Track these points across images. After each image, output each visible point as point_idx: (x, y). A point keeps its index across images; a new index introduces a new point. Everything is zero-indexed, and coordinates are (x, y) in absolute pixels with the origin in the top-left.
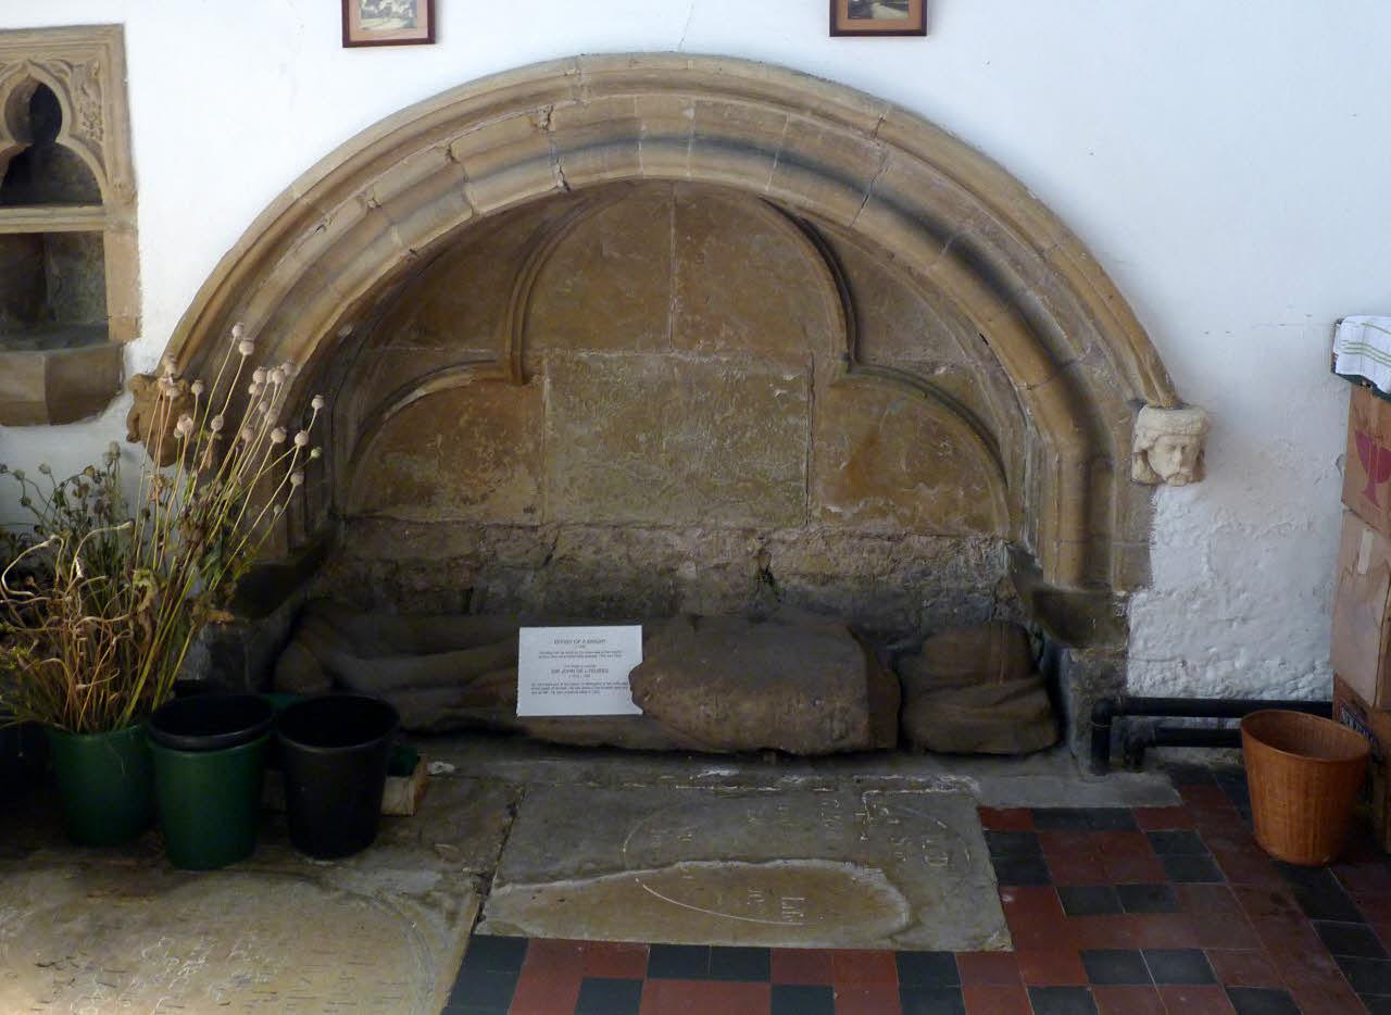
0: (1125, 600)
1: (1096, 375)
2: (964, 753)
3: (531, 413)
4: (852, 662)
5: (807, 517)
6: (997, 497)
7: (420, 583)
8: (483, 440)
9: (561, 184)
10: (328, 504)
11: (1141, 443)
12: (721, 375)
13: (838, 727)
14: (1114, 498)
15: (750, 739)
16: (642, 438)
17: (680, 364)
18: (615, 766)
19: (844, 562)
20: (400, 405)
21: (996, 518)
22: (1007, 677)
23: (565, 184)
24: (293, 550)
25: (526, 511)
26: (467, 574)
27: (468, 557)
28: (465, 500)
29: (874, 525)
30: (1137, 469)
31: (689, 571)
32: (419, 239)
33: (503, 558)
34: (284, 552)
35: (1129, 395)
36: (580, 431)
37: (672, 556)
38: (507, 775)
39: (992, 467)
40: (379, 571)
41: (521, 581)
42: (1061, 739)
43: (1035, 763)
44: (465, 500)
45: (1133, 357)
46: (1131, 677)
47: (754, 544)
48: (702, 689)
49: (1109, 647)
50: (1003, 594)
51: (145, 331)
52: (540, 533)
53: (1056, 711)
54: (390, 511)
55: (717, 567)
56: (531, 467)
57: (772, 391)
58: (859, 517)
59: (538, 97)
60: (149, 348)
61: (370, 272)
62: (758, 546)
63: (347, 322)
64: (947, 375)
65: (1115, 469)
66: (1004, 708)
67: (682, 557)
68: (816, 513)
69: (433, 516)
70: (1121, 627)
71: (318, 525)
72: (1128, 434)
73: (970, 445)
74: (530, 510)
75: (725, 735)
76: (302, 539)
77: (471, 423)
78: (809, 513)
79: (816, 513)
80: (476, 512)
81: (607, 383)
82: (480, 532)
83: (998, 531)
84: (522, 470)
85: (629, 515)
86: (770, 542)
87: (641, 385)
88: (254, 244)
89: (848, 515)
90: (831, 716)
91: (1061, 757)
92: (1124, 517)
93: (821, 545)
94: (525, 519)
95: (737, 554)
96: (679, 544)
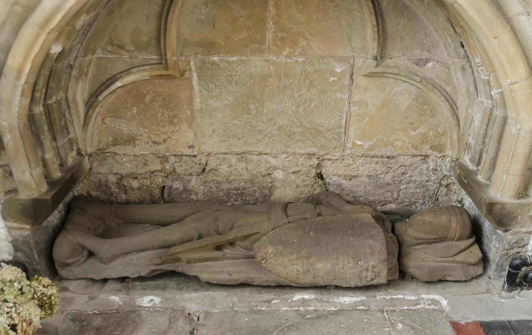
10: (75, 148)
12: (298, 69)
13: (370, 275)
16: (252, 107)
21: (448, 146)
22: (459, 239)
24: (52, 184)
25: (190, 147)
31: (279, 175)
34: (45, 188)
39: (454, 122)
40: (113, 179)
41: (190, 181)
44: (155, 143)
45: (507, 37)
48: (294, 256)
50: (444, 182)
52: (198, 158)
53: (485, 260)
54: (112, 149)
55: (294, 173)
61: (57, 9)
62: (316, 162)
64: (434, 67)
66: (459, 258)
67: (275, 168)
68: (349, 145)
75: (308, 279)
76: (57, 174)
77: (152, 101)
81: (231, 75)
82: (164, 159)
85: (246, 148)
86: (323, 160)
89: (366, 146)
90: (367, 270)
94: (189, 152)
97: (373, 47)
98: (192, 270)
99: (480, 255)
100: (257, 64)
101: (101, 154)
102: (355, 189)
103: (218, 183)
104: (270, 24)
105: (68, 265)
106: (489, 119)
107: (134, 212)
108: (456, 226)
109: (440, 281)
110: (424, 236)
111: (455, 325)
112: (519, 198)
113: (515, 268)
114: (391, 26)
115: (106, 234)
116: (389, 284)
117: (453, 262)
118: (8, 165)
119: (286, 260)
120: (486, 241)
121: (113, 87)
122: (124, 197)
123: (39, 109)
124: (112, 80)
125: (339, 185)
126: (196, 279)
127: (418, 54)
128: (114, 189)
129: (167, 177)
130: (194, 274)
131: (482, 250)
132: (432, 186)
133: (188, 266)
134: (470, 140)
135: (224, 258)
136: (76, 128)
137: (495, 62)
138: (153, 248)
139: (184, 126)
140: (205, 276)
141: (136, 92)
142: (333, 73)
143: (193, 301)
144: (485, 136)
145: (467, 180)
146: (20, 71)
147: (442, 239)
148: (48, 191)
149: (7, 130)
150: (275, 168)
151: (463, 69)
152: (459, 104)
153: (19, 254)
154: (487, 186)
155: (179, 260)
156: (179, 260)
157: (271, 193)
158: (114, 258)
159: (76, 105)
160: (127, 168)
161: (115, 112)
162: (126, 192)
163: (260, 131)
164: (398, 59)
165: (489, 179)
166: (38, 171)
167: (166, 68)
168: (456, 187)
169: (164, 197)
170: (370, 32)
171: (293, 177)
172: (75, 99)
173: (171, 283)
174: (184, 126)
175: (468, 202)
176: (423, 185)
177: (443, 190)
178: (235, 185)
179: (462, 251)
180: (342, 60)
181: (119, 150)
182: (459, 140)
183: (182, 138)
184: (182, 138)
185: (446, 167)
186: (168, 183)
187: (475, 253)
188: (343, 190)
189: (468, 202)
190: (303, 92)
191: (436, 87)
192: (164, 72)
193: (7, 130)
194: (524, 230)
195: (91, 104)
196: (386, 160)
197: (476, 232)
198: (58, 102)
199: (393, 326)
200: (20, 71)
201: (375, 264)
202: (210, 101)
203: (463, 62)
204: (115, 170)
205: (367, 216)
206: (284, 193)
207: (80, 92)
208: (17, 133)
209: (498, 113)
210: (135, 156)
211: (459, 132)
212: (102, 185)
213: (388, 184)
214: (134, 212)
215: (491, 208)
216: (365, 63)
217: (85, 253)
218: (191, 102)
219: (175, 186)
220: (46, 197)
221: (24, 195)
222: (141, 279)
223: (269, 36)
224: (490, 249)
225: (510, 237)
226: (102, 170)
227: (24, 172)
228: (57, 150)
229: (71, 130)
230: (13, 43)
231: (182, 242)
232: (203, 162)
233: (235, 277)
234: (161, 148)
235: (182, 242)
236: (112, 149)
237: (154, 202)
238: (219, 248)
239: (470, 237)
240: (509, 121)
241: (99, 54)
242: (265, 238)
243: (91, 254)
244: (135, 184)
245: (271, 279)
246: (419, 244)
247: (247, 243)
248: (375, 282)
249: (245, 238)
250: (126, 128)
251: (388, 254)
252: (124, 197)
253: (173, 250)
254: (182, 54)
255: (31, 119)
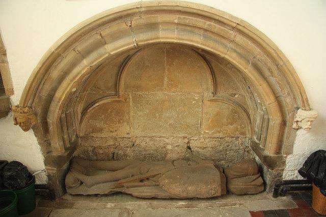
0: (286, 157)
1: (287, 100)
2: (244, 194)
3: (127, 109)
4: (216, 175)
5: (200, 133)
6: (248, 128)
7: (101, 152)
8: (115, 116)
9: (135, 45)
10: (75, 134)
11: (298, 119)
12: (178, 98)
13: (213, 192)
14: (286, 132)
15: (190, 196)
16: (157, 115)
17: (167, 95)
18: (155, 203)
19: (208, 144)
20: (91, 108)
21: (247, 133)
22: (253, 175)
23: (137, 44)
24: (66, 149)
25: (127, 134)
26: (113, 149)
27: (113, 145)
28: (111, 132)
29: (217, 135)
30: (295, 126)
31: (169, 147)
32: (93, 63)
33: (122, 145)
34: (64, 151)
35: (295, 106)
36: (140, 113)
37: (165, 144)
38: (128, 207)
39: (248, 121)
40: (90, 149)
41: (127, 150)
42: (265, 190)
43: (258, 196)
44: (111, 132)
45: (265, 85)
46: (284, 174)
47: (187, 140)
48: (178, 184)
49: (280, 168)
50: (247, 150)
51: (15, 92)
52: (131, 139)
53: (265, 184)
54: (92, 135)
55: (177, 146)
56: (128, 123)
57: (191, 102)
58: (214, 133)
59: (128, 15)
60: (16, 99)
61: (79, 73)
62: (187, 141)
63: (74, 87)
64: (238, 97)
65: (287, 125)
66: (253, 183)
67: (168, 144)
68: (202, 133)
69: (103, 135)
70: (284, 163)
71: (73, 139)
72: (293, 117)
73: (244, 115)
74: (128, 134)
75: (184, 195)
76: (68, 145)
77: (111, 112)
78: (200, 133)
79: (202, 133)
80: (114, 134)
81: (148, 101)
82: (115, 139)
83: (248, 136)
84: (125, 124)
85: (154, 135)
86: (190, 140)
87: (157, 101)
88: (42, 66)
89: (210, 133)
90: (212, 189)
91: (265, 194)
92: (288, 138)
93: (203, 140)
94: (127, 136)
95: (182, 143)
96: (167, 141)
97: (211, 87)
98: (129, 191)
99: (263, 181)
100: (160, 95)
101: (86, 137)
102: (206, 154)
103: (140, 151)
104: (166, 79)
105: (72, 187)
106: (263, 120)
107: (101, 164)
108: (251, 168)
109: (245, 194)
110: (237, 174)
111: (252, 213)
112: (277, 154)
113: (277, 186)
114: (218, 79)
115: (88, 174)
116: (222, 196)
117: (250, 185)
118: (49, 140)
119: (174, 185)
120: (265, 175)
121: (94, 106)
122: (95, 158)
123: (64, 115)
124: (94, 103)
125: (198, 152)
126: (131, 195)
127: (231, 91)
128: (91, 154)
129: (116, 148)
130: (130, 193)
131: (263, 180)
132: (242, 152)
133: (128, 189)
134: (256, 129)
135: (144, 186)
136: (76, 124)
137: (262, 95)
138: (111, 181)
139: (125, 124)
140: (135, 194)
141: (104, 108)
142: (194, 99)
143: (130, 205)
144: (262, 127)
145: (256, 148)
146: (60, 99)
147: (246, 175)
148: (65, 153)
149: (51, 124)
150: (168, 144)
151: (251, 98)
152: (250, 113)
153: (50, 182)
154: (264, 150)
155: (123, 187)
156: (123, 187)
157: (166, 156)
158: (92, 185)
159: (77, 114)
160: (97, 143)
161: (94, 117)
162: (96, 155)
163: (161, 126)
164: (222, 93)
165: (264, 146)
166: (62, 143)
167: (119, 97)
168: (252, 152)
169: (114, 157)
170: (210, 82)
171: (176, 148)
172: (77, 111)
173: (119, 198)
174: (125, 124)
175: (257, 159)
176: (237, 151)
177: (246, 153)
178: (148, 152)
179: (254, 180)
180: (198, 93)
181: (94, 135)
182: (251, 129)
183: (124, 130)
184: (124, 130)
185: (248, 143)
186: (116, 151)
187: (260, 180)
188: (199, 154)
189: (257, 159)
190: (181, 108)
191: (239, 105)
192: (117, 99)
193: (51, 124)
194: (280, 168)
195: (84, 113)
196: (220, 139)
197: (260, 171)
198: (70, 113)
199: (224, 215)
200: (60, 99)
201: (215, 187)
202: (138, 112)
203: (251, 95)
204: (92, 145)
205: (211, 165)
206: (172, 156)
207: (80, 108)
208: (55, 126)
209: (266, 117)
210: (102, 138)
211: (251, 126)
212: (86, 152)
213: (221, 151)
214: (101, 164)
215: (266, 159)
216: (208, 95)
217: (79, 183)
218: (128, 113)
219: (119, 153)
220: (64, 155)
221: (55, 154)
222: (105, 195)
223: (165, 83)
224: (267, 178)
225: (274, 172)
226: (86, 145)
227: (56, 143)
228: (68, 134)
229: (74, 125)
230: (58, 87)
231: (124, 178)
232: (134, 141)
233: (148, 194)
234: (114, 134)
235: (124, 178)
236: (92, 135)
237: (109, 160)
238: (142, 181)
239: (258, 174)
240: (270, 120)
241: (89, 92)
242: (164, 176)
243: (82, 183)
244: (101, 152)
245: (167, 195)
246: (236, 178)
247: (155, 178)
248: (215, 195)
249: (154, 176)
250: (99, 124)
251: (221, 182)
252: (95, 158)
253: (120, 181)
254: (126, 91)
255: (60, 119)
